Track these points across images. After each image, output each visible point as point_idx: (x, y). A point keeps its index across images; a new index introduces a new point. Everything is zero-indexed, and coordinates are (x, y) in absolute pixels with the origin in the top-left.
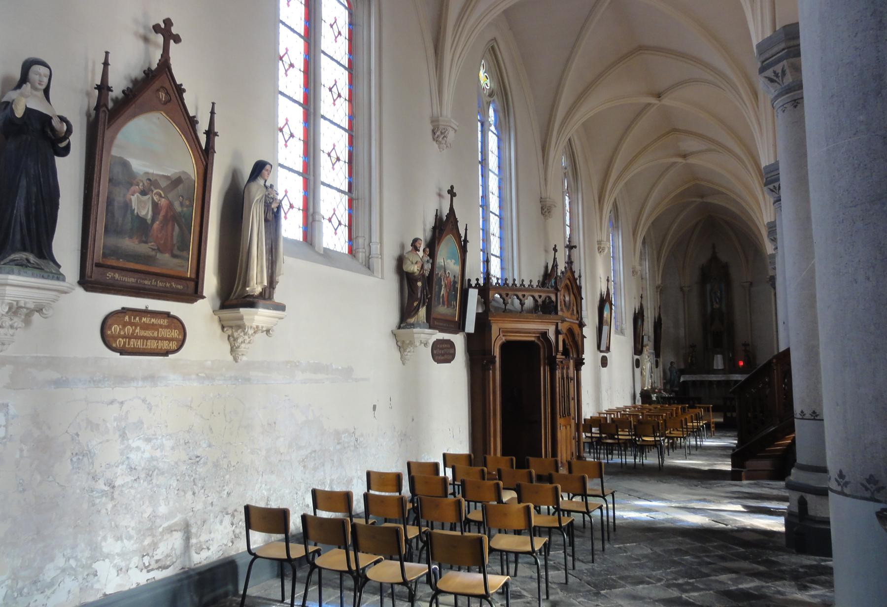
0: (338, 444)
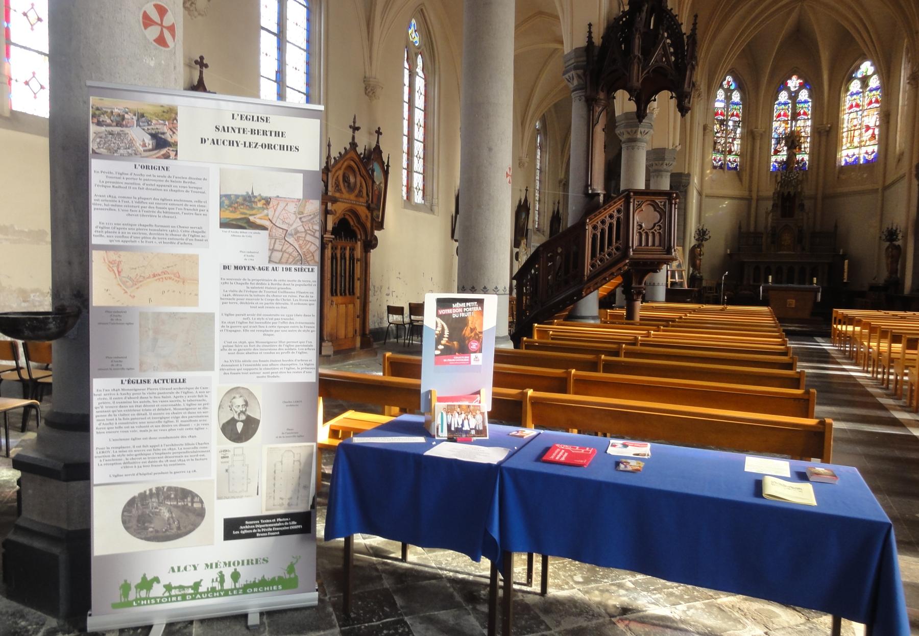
0: (24, 301)
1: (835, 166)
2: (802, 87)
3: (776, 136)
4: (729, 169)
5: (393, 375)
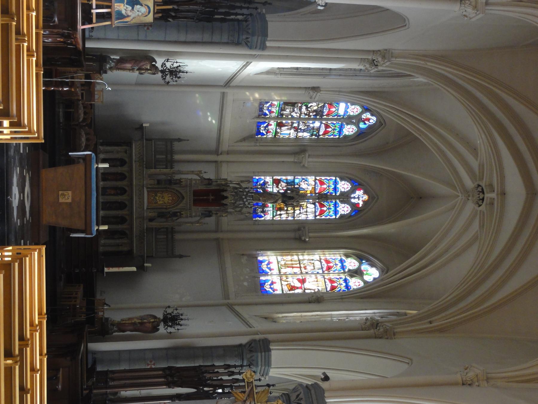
1: (257, 250)
2: (354, 206)
3: (297, 181)
4: (259, 125)
5: (102, 188)
